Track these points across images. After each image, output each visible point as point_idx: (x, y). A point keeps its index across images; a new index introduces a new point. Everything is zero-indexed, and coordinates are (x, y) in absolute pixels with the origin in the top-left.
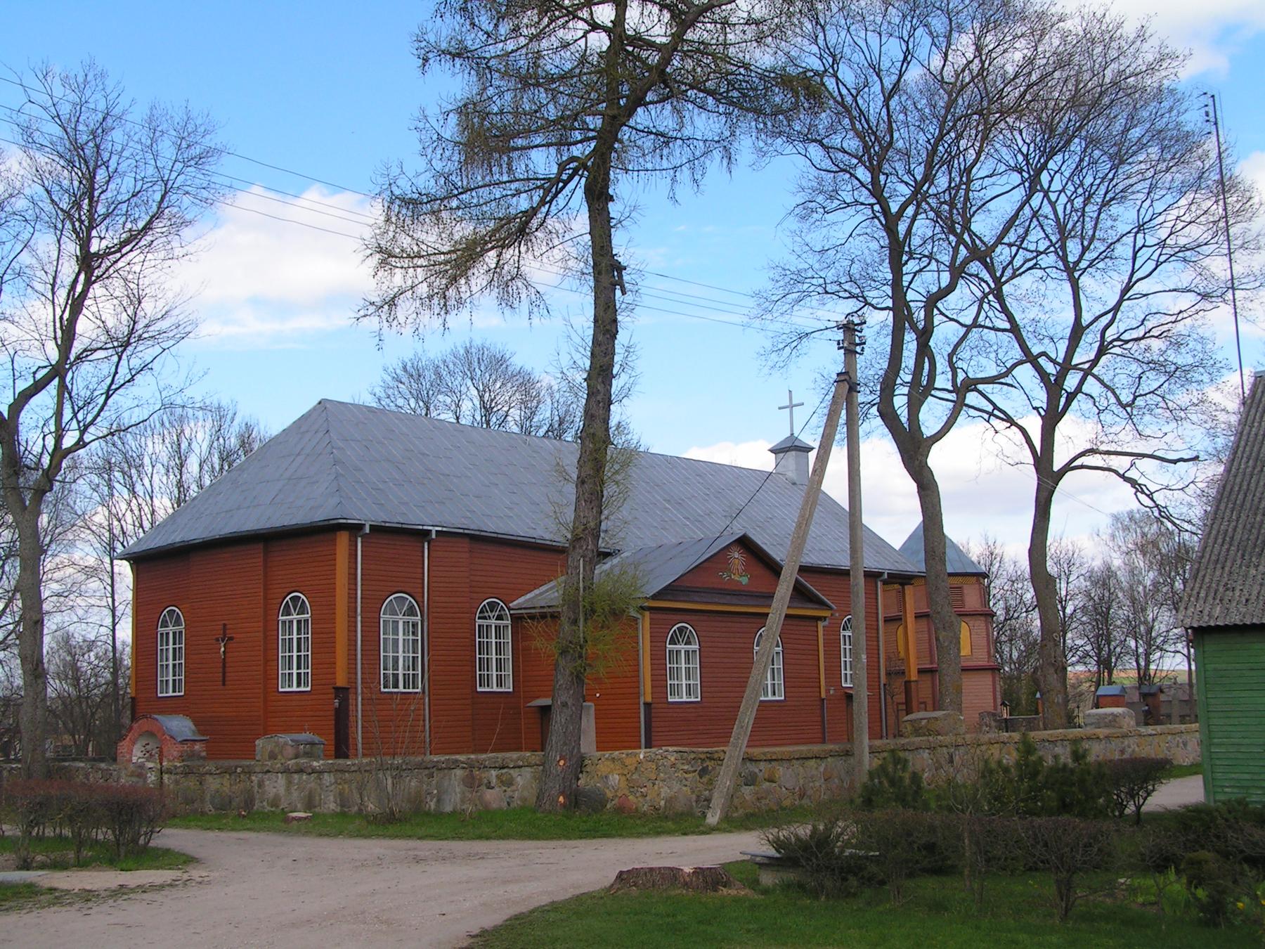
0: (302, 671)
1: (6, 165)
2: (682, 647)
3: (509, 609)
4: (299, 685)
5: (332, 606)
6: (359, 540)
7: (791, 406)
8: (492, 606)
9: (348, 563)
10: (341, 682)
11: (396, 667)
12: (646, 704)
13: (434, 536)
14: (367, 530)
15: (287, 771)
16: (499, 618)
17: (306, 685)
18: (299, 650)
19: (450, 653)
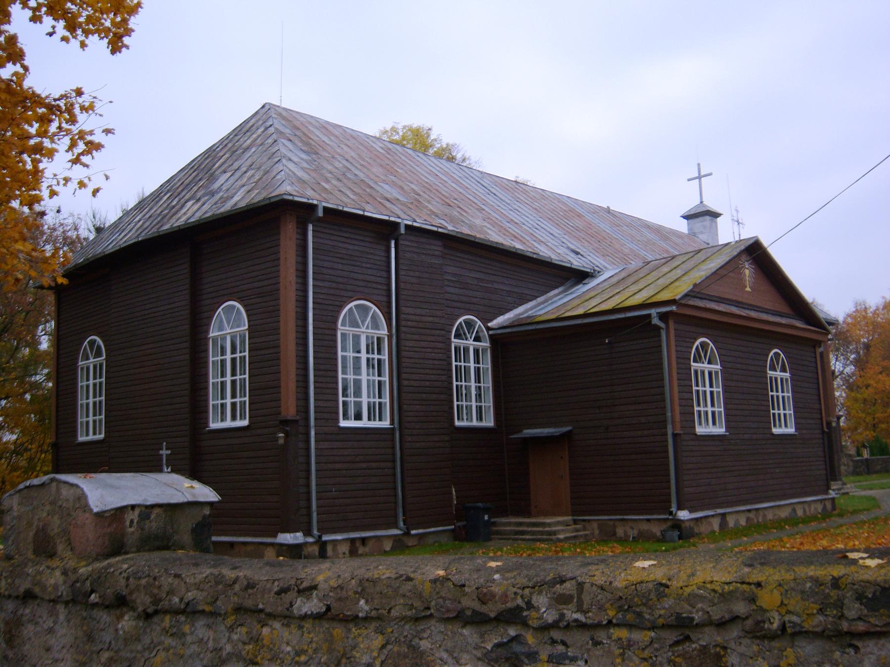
0: (238, 400)
1: (109, 127)
2: (705, 366)
3: (488, 329)
4: (234, 418)
5: (275, 312)
6: (310, 227)
7: (700, 177)
8: (469, 324)
9: (296, 257)
10: (290, 409)
11: (358, 393)
12: (675, 436)
13: (403, 231)
14: (320, 213)
15: (76, 599)
16: (477, 339)
17: (242, 417)
18: (234, 374)
19: (420, 381)
